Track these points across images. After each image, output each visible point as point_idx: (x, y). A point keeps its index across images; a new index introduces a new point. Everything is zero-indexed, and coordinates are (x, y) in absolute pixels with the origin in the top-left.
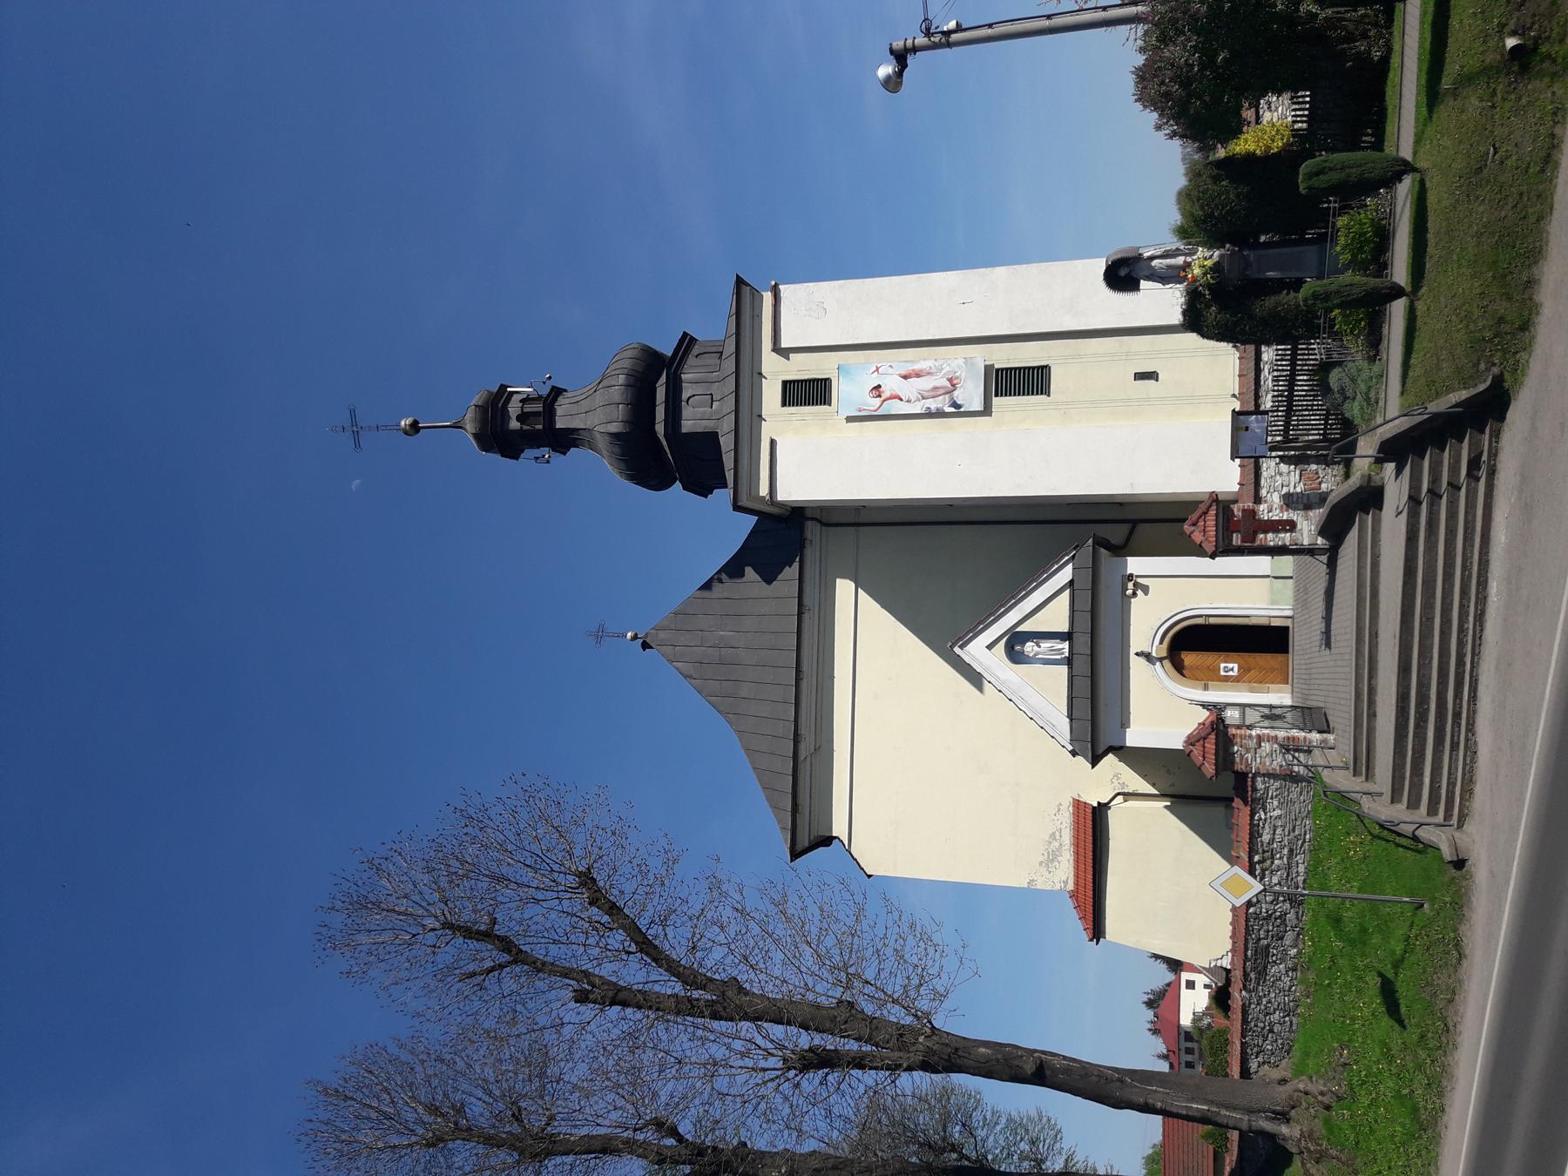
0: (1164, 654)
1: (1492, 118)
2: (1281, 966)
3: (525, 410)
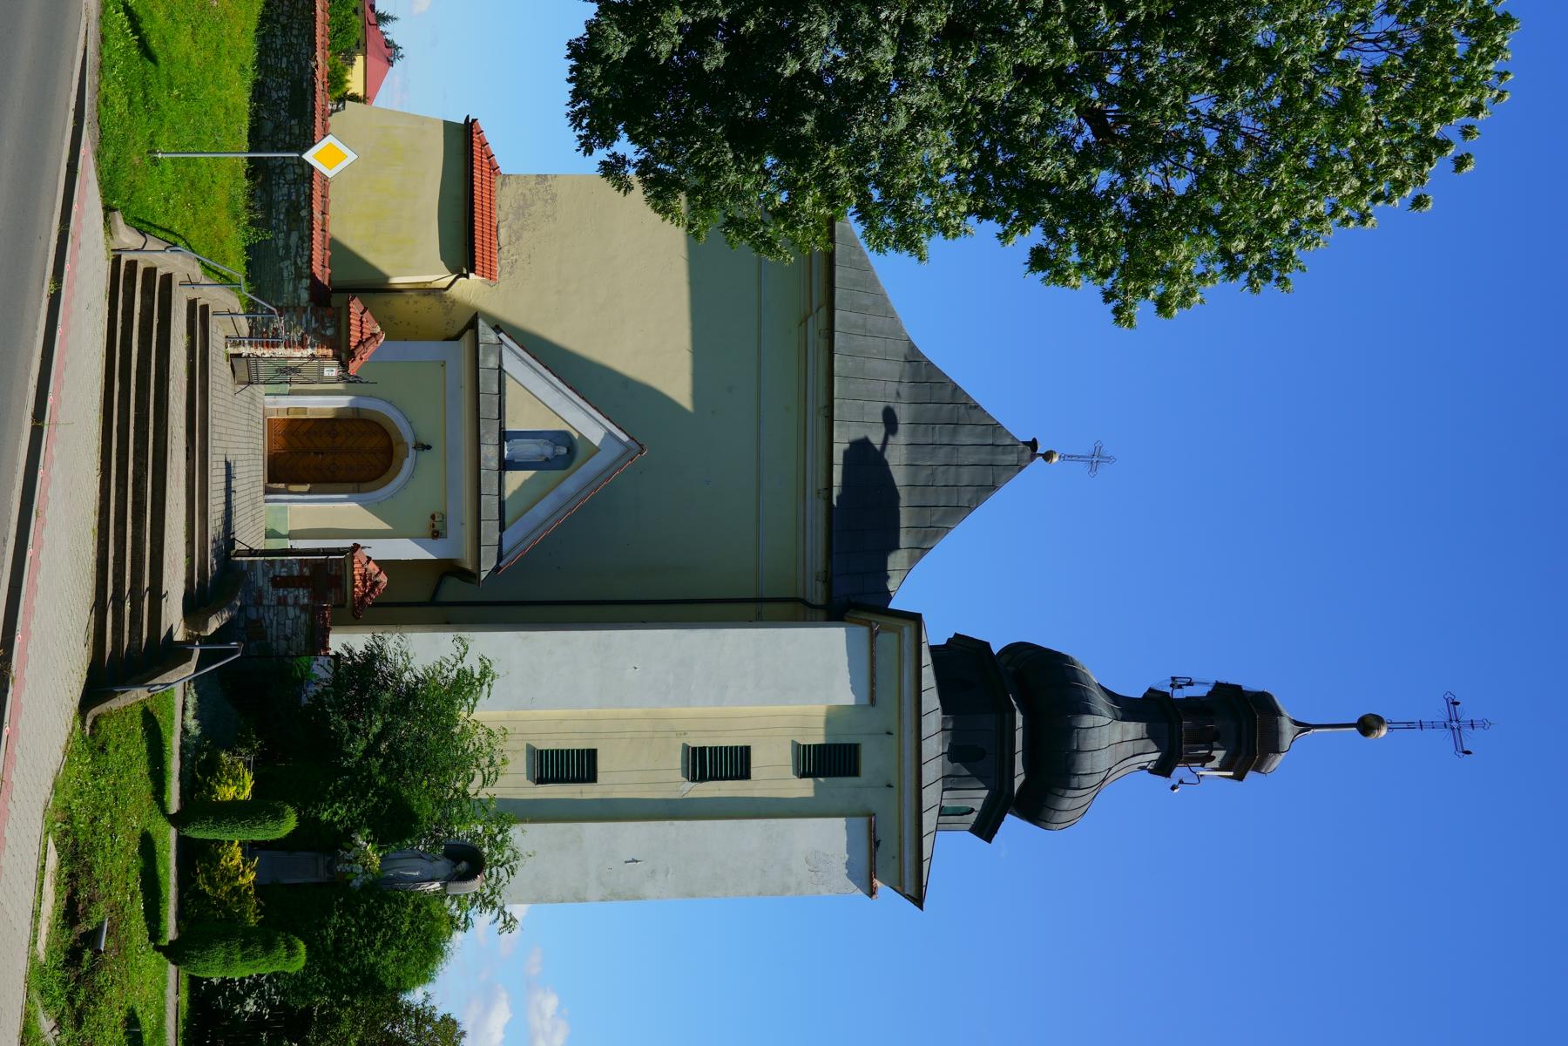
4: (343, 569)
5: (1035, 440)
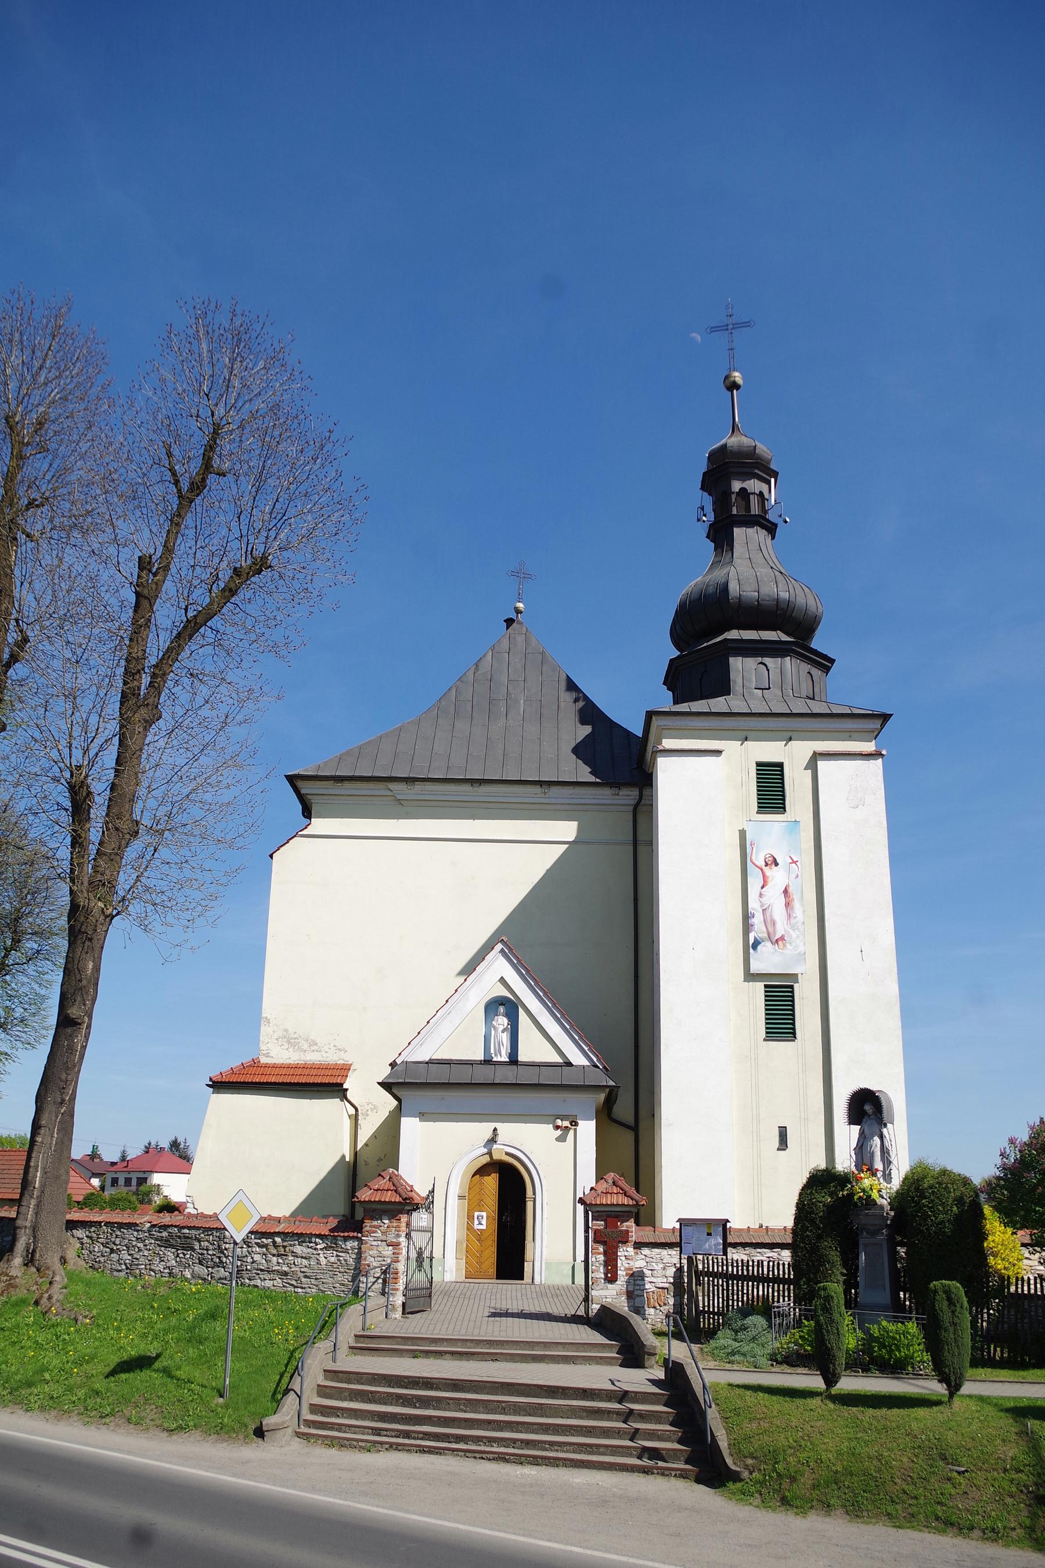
0: (496, 1157)
1: (994, 1470)
2: (174, 1262)
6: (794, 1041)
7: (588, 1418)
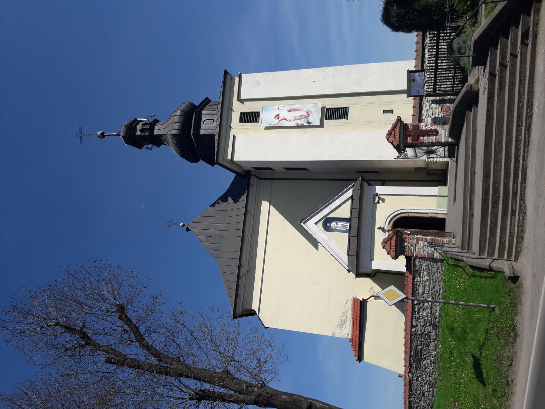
0: (390, 229)
2: (428, 361)
3: (143, 127)
4: (404, 138)
5: (187, 231)
6: (348, 108)
7: (504, 91)
